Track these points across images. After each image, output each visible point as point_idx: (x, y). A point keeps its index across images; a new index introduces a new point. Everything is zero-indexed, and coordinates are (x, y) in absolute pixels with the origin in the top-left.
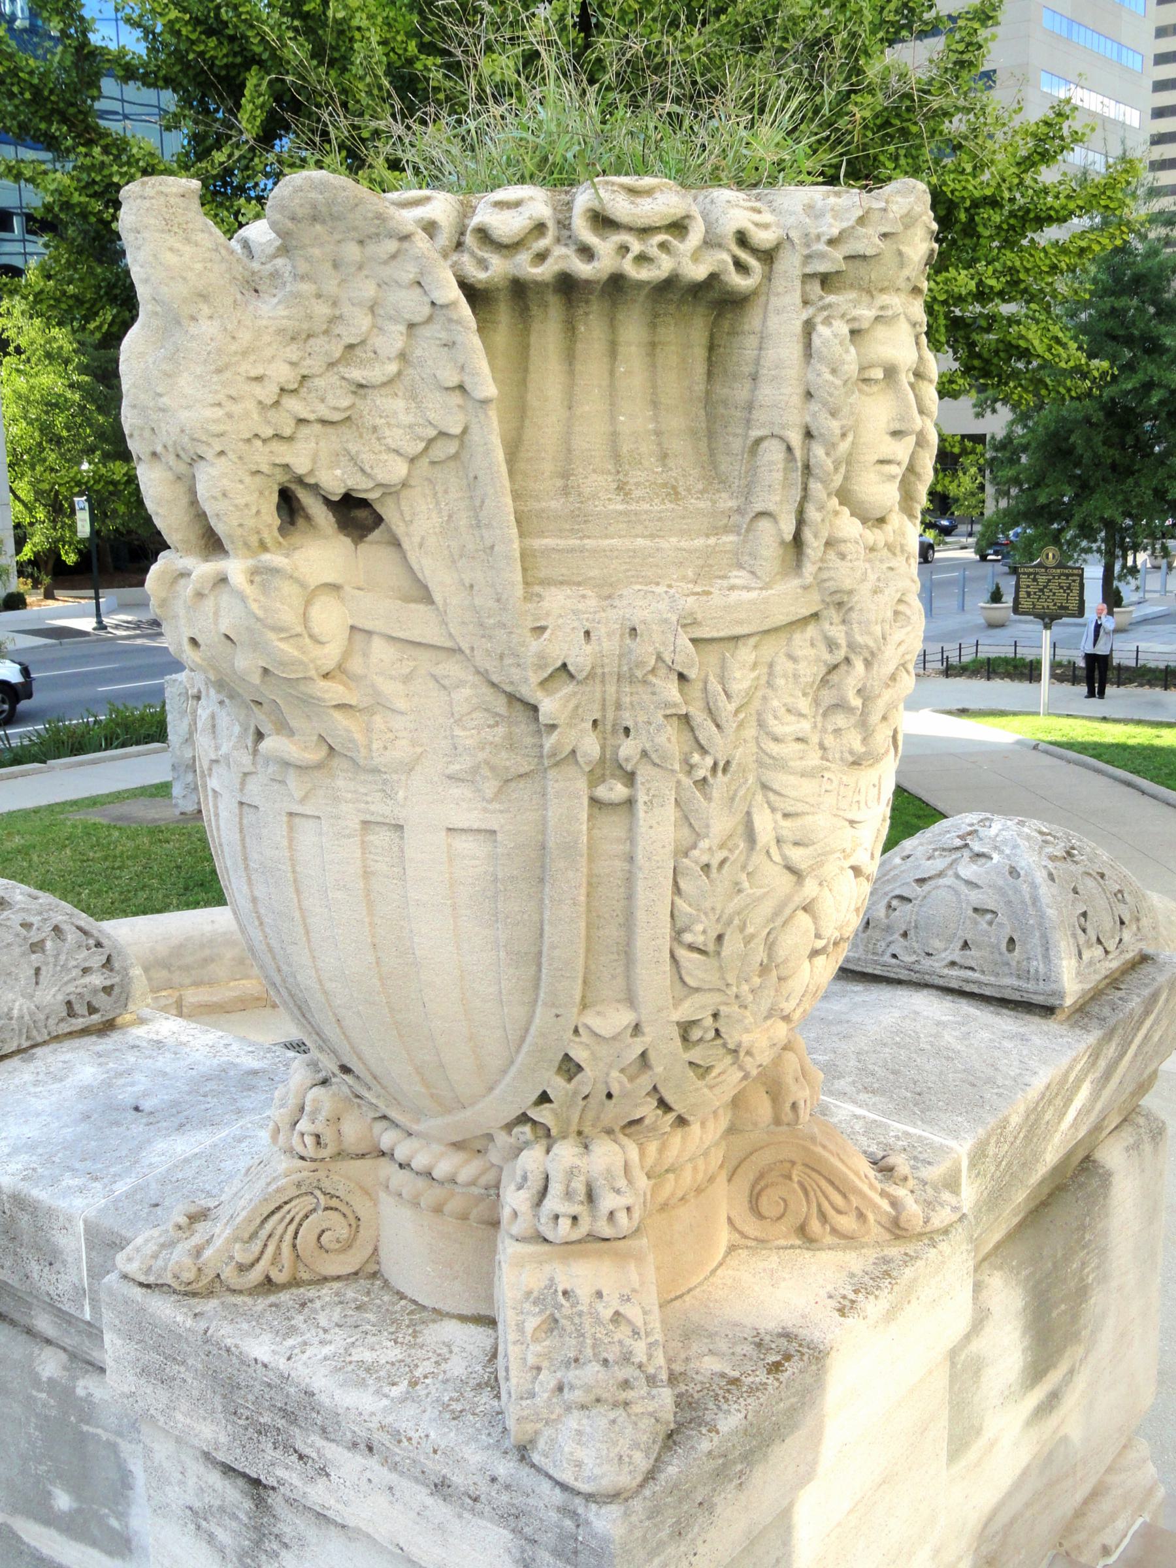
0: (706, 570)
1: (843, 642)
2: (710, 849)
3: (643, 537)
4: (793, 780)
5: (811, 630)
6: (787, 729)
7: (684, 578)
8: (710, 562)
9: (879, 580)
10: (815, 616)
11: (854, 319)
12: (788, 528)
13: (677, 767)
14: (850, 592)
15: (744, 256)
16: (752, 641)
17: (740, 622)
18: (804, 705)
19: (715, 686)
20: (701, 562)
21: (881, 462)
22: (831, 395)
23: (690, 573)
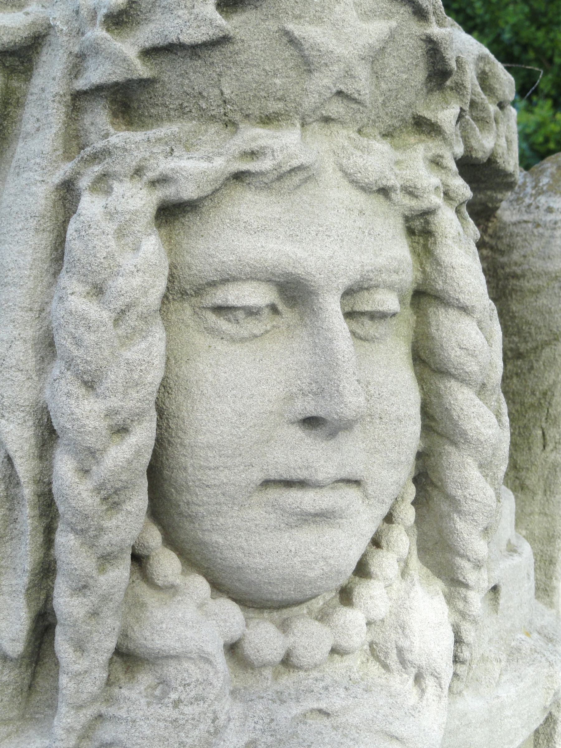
11: (162, 180)
21: (267, 483)
22: (78, 342)
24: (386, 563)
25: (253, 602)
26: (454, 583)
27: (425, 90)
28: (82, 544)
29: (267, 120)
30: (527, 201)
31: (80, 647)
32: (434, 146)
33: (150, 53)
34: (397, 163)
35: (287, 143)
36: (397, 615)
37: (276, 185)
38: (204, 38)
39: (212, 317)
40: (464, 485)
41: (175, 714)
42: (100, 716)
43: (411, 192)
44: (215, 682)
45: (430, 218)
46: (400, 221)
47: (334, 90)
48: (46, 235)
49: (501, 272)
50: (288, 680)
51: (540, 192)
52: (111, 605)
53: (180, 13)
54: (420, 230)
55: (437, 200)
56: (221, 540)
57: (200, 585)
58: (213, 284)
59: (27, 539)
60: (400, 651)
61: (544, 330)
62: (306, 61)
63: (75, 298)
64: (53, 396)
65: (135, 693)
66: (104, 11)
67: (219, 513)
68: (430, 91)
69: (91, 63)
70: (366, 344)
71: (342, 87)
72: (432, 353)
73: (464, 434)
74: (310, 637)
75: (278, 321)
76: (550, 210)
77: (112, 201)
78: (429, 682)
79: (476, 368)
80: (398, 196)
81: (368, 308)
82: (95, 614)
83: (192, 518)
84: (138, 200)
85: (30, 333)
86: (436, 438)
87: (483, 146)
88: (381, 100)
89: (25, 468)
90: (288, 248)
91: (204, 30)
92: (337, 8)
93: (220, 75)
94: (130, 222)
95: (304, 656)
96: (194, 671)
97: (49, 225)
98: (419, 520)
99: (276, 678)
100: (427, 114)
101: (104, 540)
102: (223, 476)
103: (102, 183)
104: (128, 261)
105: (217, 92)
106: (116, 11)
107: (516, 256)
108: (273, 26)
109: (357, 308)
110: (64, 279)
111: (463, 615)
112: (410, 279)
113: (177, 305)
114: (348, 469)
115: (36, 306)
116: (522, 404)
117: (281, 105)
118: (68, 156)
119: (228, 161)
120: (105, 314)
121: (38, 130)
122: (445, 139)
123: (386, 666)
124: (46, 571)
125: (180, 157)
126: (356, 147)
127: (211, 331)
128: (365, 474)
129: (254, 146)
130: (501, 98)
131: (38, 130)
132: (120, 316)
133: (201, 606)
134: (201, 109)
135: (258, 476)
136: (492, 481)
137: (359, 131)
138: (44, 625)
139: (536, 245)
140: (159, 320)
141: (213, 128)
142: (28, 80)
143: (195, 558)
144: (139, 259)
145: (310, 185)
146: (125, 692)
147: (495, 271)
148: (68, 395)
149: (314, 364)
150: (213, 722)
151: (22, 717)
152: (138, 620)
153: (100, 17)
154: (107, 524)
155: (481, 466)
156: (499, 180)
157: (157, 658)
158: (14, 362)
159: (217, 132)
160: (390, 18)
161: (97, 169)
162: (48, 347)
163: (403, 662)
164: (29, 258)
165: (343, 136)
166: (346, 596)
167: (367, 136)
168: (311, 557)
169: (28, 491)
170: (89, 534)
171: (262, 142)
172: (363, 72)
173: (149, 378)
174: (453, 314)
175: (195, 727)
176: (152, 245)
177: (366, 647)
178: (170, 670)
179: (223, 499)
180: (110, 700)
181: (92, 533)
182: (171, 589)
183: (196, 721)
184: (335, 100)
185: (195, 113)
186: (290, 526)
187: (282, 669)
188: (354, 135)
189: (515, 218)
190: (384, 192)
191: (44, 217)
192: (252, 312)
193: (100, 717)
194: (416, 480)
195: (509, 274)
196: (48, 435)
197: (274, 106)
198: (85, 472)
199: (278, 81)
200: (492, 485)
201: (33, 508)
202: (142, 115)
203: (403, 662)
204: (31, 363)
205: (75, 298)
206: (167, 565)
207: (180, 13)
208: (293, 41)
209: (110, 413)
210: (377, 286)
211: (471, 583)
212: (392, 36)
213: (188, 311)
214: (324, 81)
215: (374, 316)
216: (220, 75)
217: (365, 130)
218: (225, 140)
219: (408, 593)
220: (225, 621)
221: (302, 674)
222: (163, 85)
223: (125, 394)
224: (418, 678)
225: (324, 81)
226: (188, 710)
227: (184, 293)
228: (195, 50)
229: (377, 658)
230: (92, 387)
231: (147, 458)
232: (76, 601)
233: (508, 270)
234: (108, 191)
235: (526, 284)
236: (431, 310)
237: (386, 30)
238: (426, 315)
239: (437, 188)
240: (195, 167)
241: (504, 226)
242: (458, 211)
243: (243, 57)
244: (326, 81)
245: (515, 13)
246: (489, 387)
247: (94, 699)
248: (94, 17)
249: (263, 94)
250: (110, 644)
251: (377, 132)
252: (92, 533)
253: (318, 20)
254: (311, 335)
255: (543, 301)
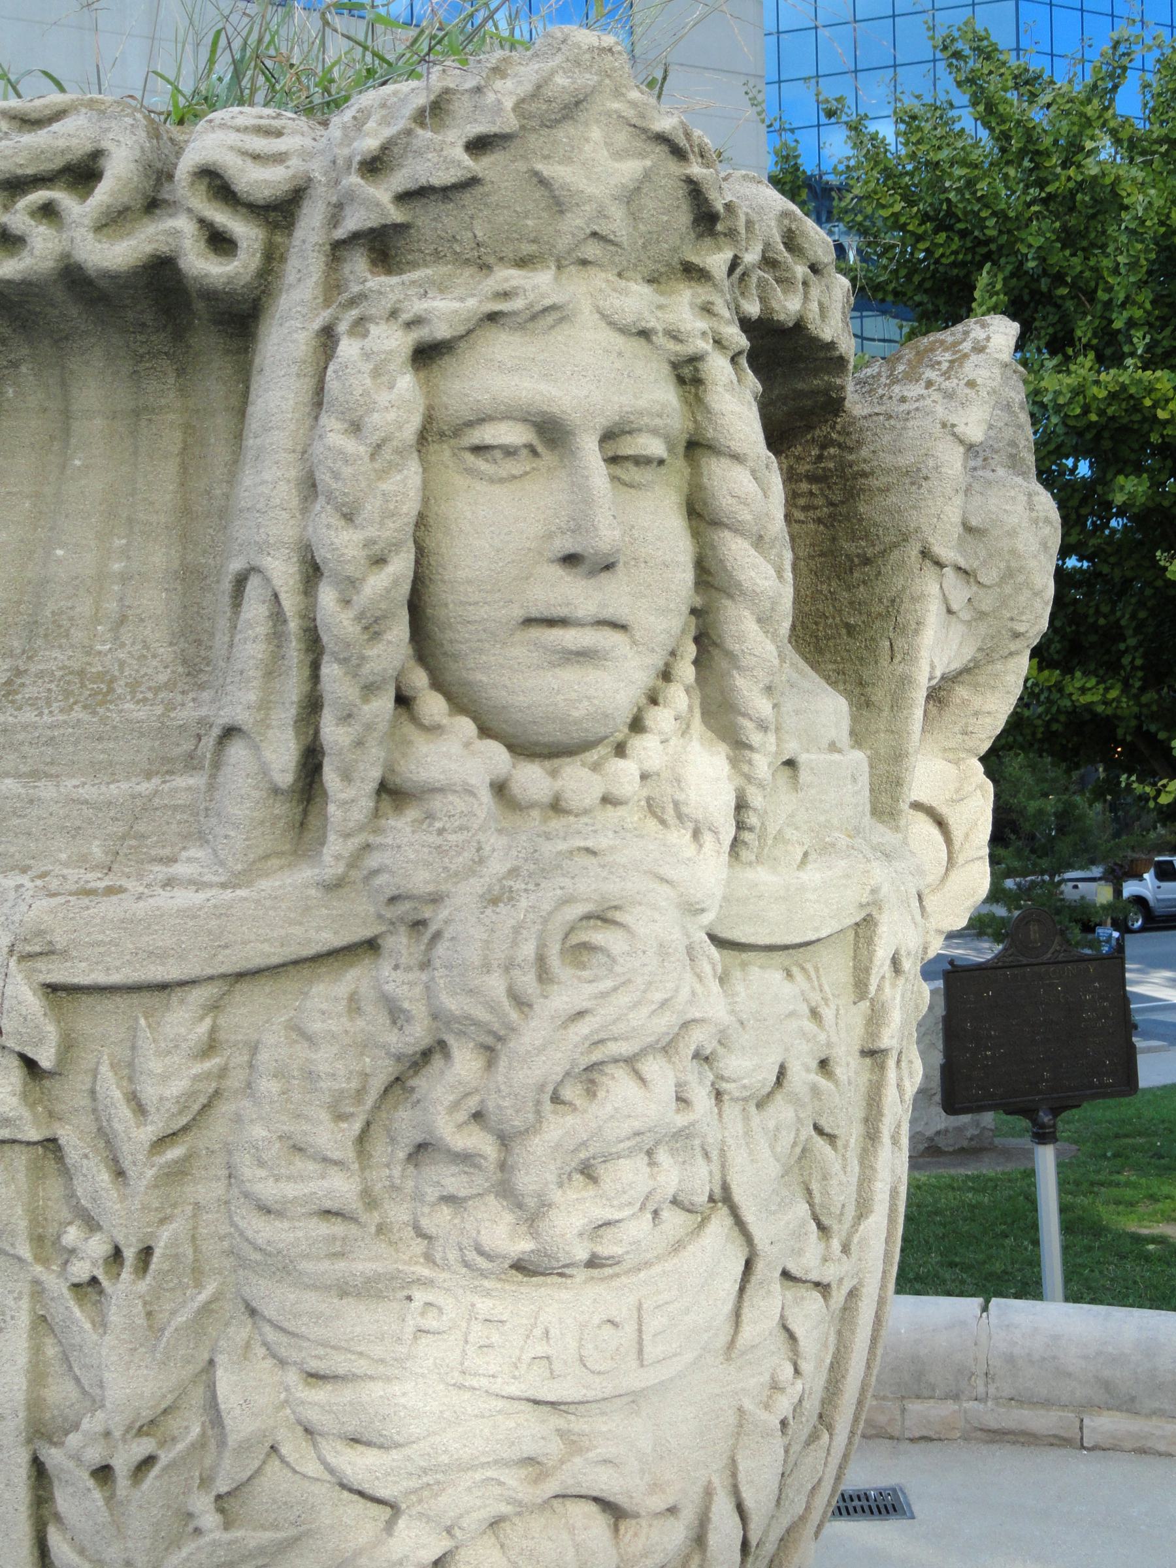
0: (135, 842)
1: (418, 1010)
2: (107, 1434)
3: (18, 776)
4: (311, 1300)
5: (355, 978)
6: (291, 1190)
7: (83, 860)
8: (141, 827)
9: (514, 872)
10: (371, 946)
11: (415, 322)
12: (282, 756)
13: (24, 1250)
14: (436, 899)
15: (222, 218)
16: (199, 996)
17: (158, 955)
18: (333, 1138)
19: (112, 1091)
20: (119, 828)
21: (529, 622)
22: (336, 476)
23: (96, 850)
24: (661, 719)
25: (524, 748)
26: (739, 746)
27: (693, 235)
28: (346, 674)
29: (523, 262)
30: (880, 391)
31: (347, 777)
32: (704, 293)
33: (404, 198)
34: (660, 307)
35: (539, 284)
36: (673, 769)
37: (530, 325)
38: (453, 180)
39: (470, 458)
40: (741, 639)
41: (439, 841)
42: (368, 845)
43: (674, 335)
44: (478, 813)
45: (700, 365)
46: (666, 369)
47: (588, 231)
48: (307, 380)
49: (848, 471)
50: (556, 824)
51: (895, 381)
52: (375, 734)
53: (430, 156)
54: (688, 376)
55: (705, 346)
56: (485, 679)
57: (466, 726)
58: (470, 424)
59: (294, 672)
60: (676, 804)
61: (892, 531)
62: (559, 203)
63: (334, 434)
64: (315, 531)
65: (401, 826)
66: (358, 158)
67: (481, 651)
68: (700, 236)
69: (348, 211)
70: (632, 491)
71: (596, 228)
72: (705, 504)
73: (739, 584)
74: (577, 780)
75: (538, 463)
76: (903, 400)
77: (368, 343)
78: (708, 838)
79: (749, 517)
80: (660, 339)
81: (630, 452)
82: (359, 743)
83: (455, 657)
84: (394, 341)
85: (293, 473)
86: (714, 593)
87: (785, 307)
88: (640, 242)
89: (290, 603)
90: (543, 387)
91: (452, 171)
92: (587, 148)
93: (472, 218)
94: (386, 361)
95: (573, 800)
96: (458, 803)
97: (310, 370)
98: (701, 680)
99: (545, 821)
100: (695, 259)
101: (366, 669)
102: (483, 612)
103: (360, 326)
104: (383, 398)
105: (470, 235)
106: (368, 158)
107: (864, 452)
108: (521, 166)
109: (620, 453)
110: (324, 419)
111: (749, 778)
112: (678, 426)
113: (436, 446)
114: (611, 610)
115: (299, 448)
116: (869, 614)
117: (534, 247)
118: (327, 302)
119: (481, 302)
120: (362, 449)
121: (299, 280)
122: (715, 285)
123: (663, 822)
124: (313, 706)
125: (433, 298)
126: (614, 290)
127: (469, 471)
128: (631, 618)
129: (507, 286)
130: (813, 259)
131: (299, 280)
132: (377, 450)
133: (467, 745)
134: (456, 253)
135: (518, 613)
136: (774, 636)
137: (620, 275)
138: (311, 761)
139: (887, 438)
140: (415, 455)
141: (468, 271)
142: (290, 235)
143: (461, 701)
144: (393, 396)
145: (565, 326)
146: (392, 822)
147: (843, 471)
148: (329, 526)
149: (572, 502)
150: (478, 850)
151: (295, 852)
152: (404, 755)
153: (355, 165)
154: (369, 653)
155: (759, 620)
156: (822, 355)
157: (423, 792)
158: (278, 501)
159: (472, 276)
160: (644, 157)
161: (354, 313)
162: (310, 487)
163: (680, 816)
164: (291, 402)
165: (600, 279)
166: (620, 750)
167: (628, 280)
168: (574, 696)
169: (293, 625)
170: (352, 664)
171: (514, 283)
172: (617, 212)
173: (405, 509)
174: (725, 462)
175: (459, 854)
176: (406, 382)
177: (643, 803)
178: (437, 803)
179: (484, 636)
180: (377, 831)
181: (354, 662)
182: (434, 730)
183: (460, 848)
184: (590, 241)
185: (449, 257)
186: (553, 665)
187: (551, 813)
188: (614, 278)
189: (865, 412)
190: (645, 334)
191: (305, 362)
192: (509, 452)
193: (367, 847)
194: (697, 640)
195: (857, 473)
196: (312, 572)
197: (527, 249)
198: (347, 602)
199: (529, 222)
200: (773, 641)
201: (299, 640)
202: (400, 262)
203: (680, 816)
204: (295, 502)
205: (334, 434)
206: (433, 705)
207: (430, 156)
208: (543, 182)
209: (368, 543)
210: (640, 430)
211: (755, 744)
212: (647, 176)
213: (448, 453)
214: (575, 222)
215: (641, 461)
216: (472, 218)
217: (626, 274)
218: (479, 283)
219: (684, 748)
220: (490, 758)
221: (572, 818)
222: (418, 231)
223: (382, 524)
224: (696, 834)
225: (575, 222)
226: (452, 838)
227: (442, 434)
228: (446, 192)
229: (654, 814)
230: (351, 520)
231: (406, 588)
232: (341, 730)
233: (855, 468)
234: (365, 335)
235: (875, 483)
236: (703, 461)
237: (640, 170)
238: (699, 466)
239: (704, 333)
240: (446, 307)
241: (854, 421)
242: (733, 360)
243: (493, 199)
244: (578, 222)
245: (1040, 232)
246: (767, 539)
247: (362, 828)
248: (349, 167)
249: (515, 235)
250: (376, 774)
251: (639, 277)
252: (354, 662)
253: (567, 160)
254: (569, 475)
255: (892, 499)
